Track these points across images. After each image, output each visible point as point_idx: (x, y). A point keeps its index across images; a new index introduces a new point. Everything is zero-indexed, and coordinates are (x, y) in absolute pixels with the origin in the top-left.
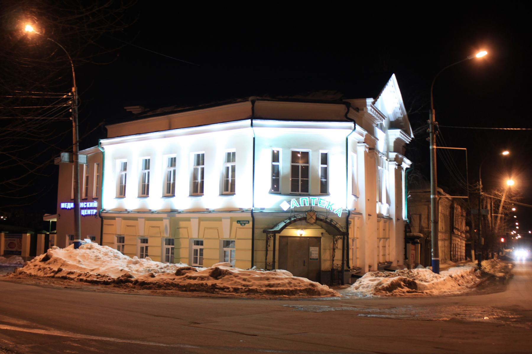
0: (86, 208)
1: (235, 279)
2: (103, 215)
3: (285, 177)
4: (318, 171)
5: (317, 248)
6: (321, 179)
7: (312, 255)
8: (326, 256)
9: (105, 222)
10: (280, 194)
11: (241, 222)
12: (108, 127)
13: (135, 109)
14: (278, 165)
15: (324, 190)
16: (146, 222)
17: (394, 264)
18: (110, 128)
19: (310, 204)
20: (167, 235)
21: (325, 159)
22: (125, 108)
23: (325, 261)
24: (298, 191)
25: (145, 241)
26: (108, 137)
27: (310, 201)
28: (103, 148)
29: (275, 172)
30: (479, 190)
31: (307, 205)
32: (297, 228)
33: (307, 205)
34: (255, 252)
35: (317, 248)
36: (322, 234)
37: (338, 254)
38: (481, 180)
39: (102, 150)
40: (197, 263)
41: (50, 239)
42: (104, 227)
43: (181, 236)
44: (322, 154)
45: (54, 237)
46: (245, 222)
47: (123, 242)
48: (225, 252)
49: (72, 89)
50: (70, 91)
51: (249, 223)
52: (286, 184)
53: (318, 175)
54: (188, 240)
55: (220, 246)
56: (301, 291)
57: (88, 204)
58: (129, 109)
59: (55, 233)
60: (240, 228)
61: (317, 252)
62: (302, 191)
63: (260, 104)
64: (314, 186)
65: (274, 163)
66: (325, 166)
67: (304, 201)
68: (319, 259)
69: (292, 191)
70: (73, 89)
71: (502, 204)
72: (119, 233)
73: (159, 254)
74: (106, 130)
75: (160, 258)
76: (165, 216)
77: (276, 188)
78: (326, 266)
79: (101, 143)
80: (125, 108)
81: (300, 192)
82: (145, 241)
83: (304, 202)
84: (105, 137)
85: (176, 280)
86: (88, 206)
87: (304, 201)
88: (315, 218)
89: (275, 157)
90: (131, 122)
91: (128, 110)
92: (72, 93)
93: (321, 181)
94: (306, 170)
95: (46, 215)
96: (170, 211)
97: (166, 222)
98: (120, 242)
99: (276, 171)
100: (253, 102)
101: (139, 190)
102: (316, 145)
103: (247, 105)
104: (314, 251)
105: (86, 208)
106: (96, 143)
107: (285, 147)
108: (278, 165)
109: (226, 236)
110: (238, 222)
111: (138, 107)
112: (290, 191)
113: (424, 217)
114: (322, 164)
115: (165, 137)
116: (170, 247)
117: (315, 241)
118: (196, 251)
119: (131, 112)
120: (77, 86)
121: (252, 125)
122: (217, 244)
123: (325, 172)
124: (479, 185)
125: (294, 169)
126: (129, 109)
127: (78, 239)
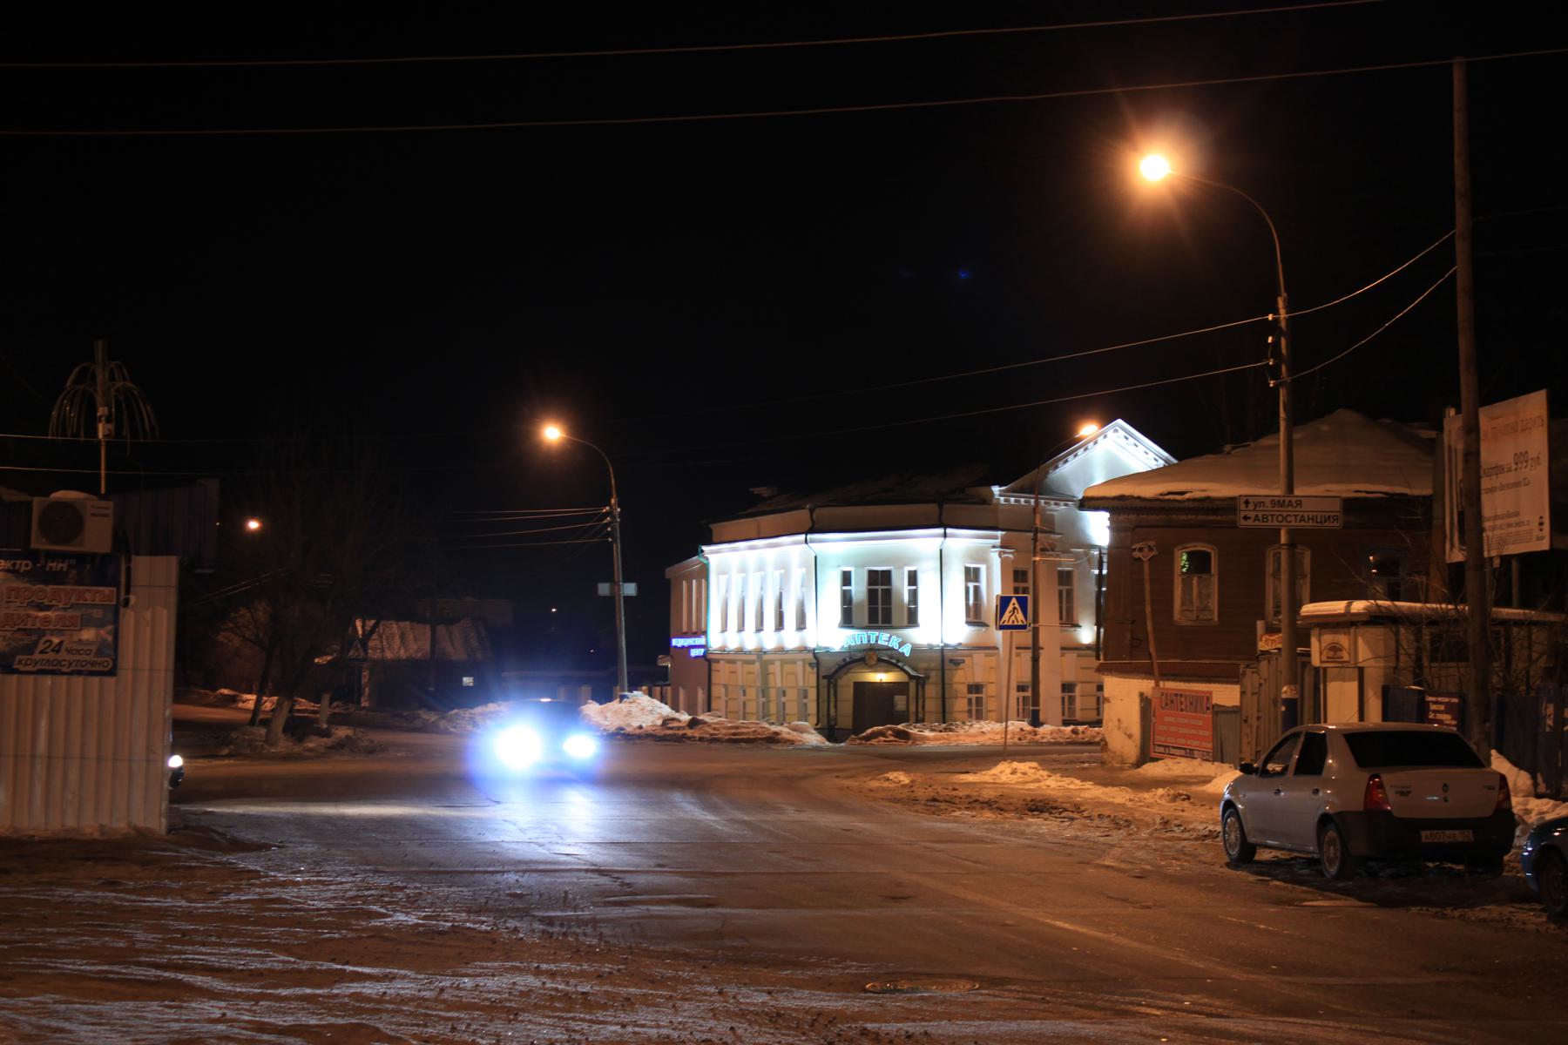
1: (707, 729)
2: (710, 657)
3: (860, 605)
4: (902, 594)
6: (909, 604)
7: (898, 707)
9: (714, 666)
10: (852, 627)
12: (712, 526)
13: (764, 491)
14: (850, 590)
15: (912, 619)
16: (745, 666)
18: (717, 528)
19: (869, 641)
21: (913, 578)
22: (751, 490)
24: (877, 623)
26: (715, 540)
27: (869, 637)
28: (707, 559)
29: (846, 598)
32: (876, 671)
33: (865, 642)
34: (940, 709)
35: (905, 697)
39: (705, 562)
44: (909, 572)
45: (666, 690)
48: (806, 704)
49: (610, 501)
50: (609, 504)
52: (862, 615)
53: (903, 600)
55: (799, 696)
56: (761, 739)
58: (757, 491)
59: (669, 685)
61: (905, 703)
62: (883, 623)
63: (824, 512)
64: (898, 615)
65: (845, 588)
66: (914, 588)
69: (870, 623)
70: (613, 501)
73: (755, 711)
74: (710, 531)
75: (755, 716)
77: (848, 620)
79: (702, 551)
80: (751, 490)
81: (880, 624)
83: (884, 638)
84: (710, 542)
85: (1009, 771)
87: (861, 638)
88: (875, 658)
89: (846, 578)
90: (747, 520)
91: (756, 493)
93: (909, 608)
94: (888, 594)
95: (660, 656)
97: (757, 667)
99: (848, 598)
100: (812, 511)
101: (776, 620)
102: (901, 560)
103: (802, 515)
106: (697, 552)
107: (859, 566)
108: (850, 590)
111: (765, 488)
112: (866, 623)
114: (910, 584)
115: (752, 548)
119: (759, 495)
120: (618, 496)
121: (806, 542)
123: (914, 596)
125: (872, 595)
126: (757, 491)
127: (624, 691)
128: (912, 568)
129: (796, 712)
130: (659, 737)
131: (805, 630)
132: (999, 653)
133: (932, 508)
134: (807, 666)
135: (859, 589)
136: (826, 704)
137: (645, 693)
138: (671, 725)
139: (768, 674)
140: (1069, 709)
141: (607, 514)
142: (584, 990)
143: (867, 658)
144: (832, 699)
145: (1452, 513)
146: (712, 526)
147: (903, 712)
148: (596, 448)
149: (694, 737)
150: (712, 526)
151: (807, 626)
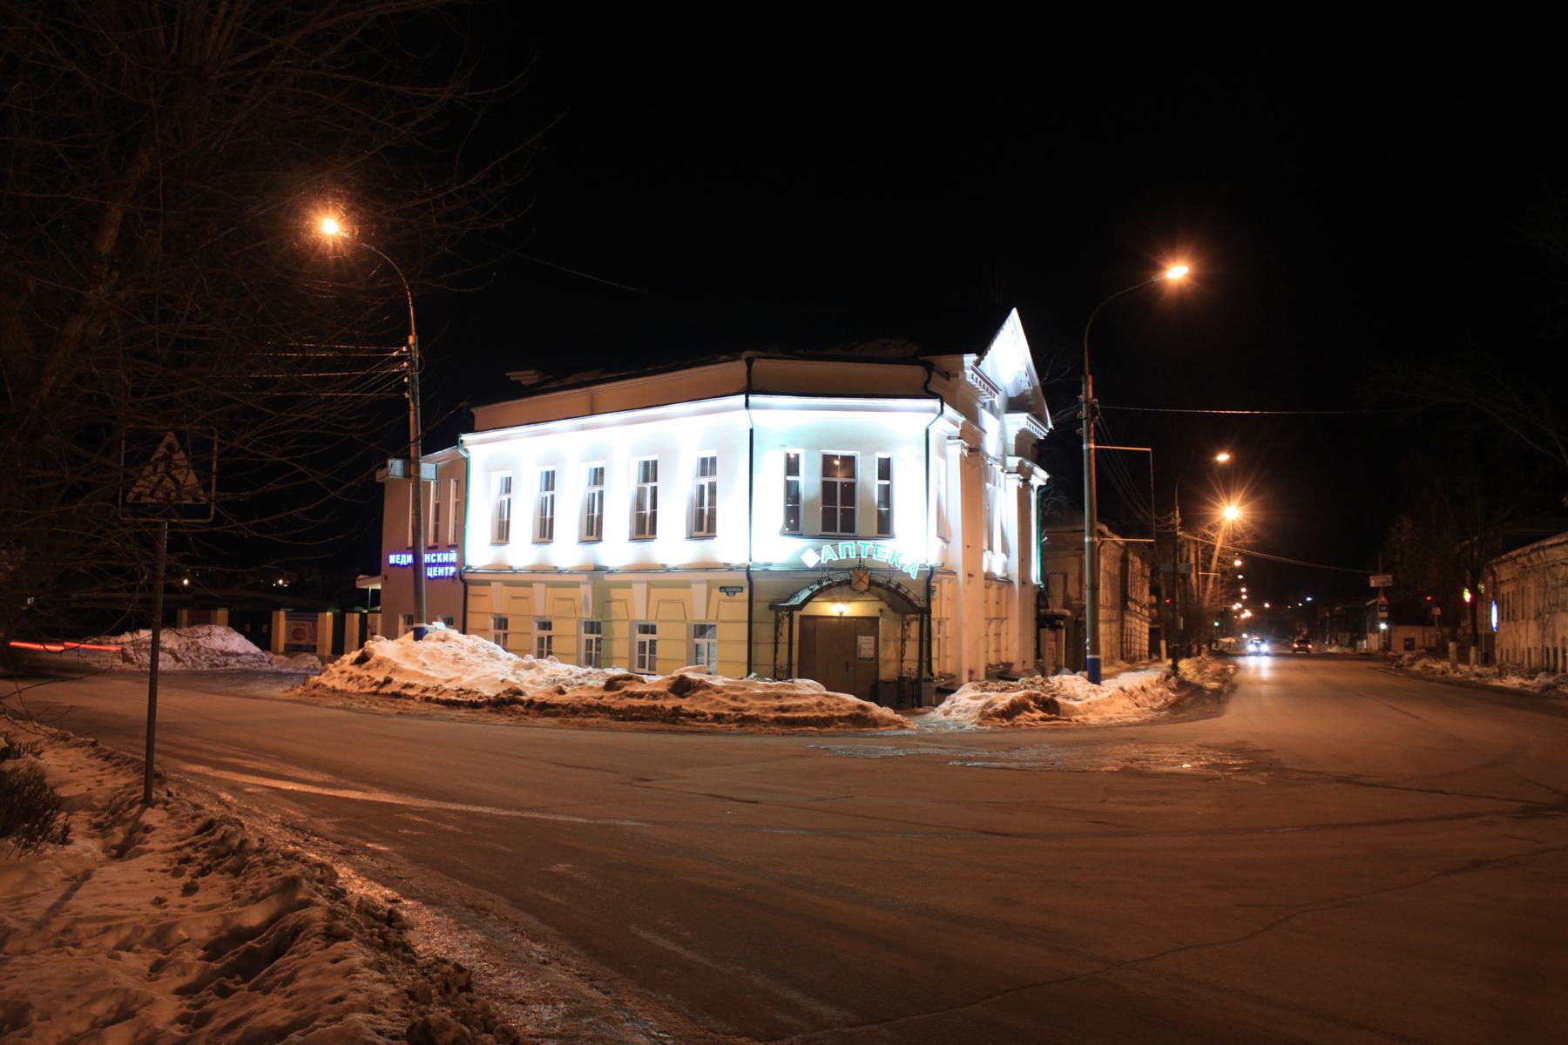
0: (434, 565)
2: (467, 577)
3: (810, 504)
4: (872, 492)
5: (872, 638)
6: (879, 507)
8: (889, 652)
9: (472, 589)
10: (801, 536)
11: (728, 590)
13: (527, 377)
14: (797, 482)
15: (884, 527)
16: (549, 589)
17: (1017, 668)
18: (480, 413)
20: (588, 615)
21: (885, 470)
23: (887, 661)
24: (836, 531)
25: (647, 629)
26: (476, 429)
27: (858, 549)
29: (792, 494)
30: (1174, 526)
31: (853, 556)
32: (835, 601)
33: (853, 556)
35: (872, 638)
36: (881, 611)
37: (912, 650)
38: (1178, 508)
40: (644, 667)
41: (369, 622)
42: (470, 599)
43: (614, 617)
46: (734, 590)
47: (506, 628)
49: (408, 340)
50: (406, 343)
51: (742, 591)
52: (812, 518)
54: (627, 625)
56: (841, 719)
57: (439, 556)
60: (725, 601)
61: (872, 646)
63: (764, 366)
64: (865, 519)
65: (790, 478)
66: (887, 482)
67: (847, 549)
68: (875, 660)
69: (824, 530)
70: (411, 340)
71: (1216, 553)
72: (497, 611)
74: (472, 417)
76: (584, 578)
77: (794, 522)
78: (888, 672)
79: (462, 441)
81: (839, 533)
82: (546, 626)
83: (846, 550)
84: (471, 429)
86: (439, 560)
87: (847, 549)
88: (866, 580)
89: (792, 466)
92: (409, 347)
94: (850, 491)
95: (361, 577)
96: (592, 569)
97: (586, 590)
98: (500, 628)
99: (793, 493)
100: (749, 362)
102: (870, 443)
104: (865, 644)
105: (434, 565)
109: (700, 616)
110: (722, 589)
112: (820, 531)
113: (1072, 578)
114: (880, 478)
115: (583, 428)
116: (593, 637)
117: (868, 625)
118: (642, 645)
120: (418, 333)
121: (747, 405)
122: (682, 632)
123: (886, 493)
124: (1175, 517)
125: (828, 489)
126: (514, 376)
128: (885, 455)
129: (685, 657)
130: (621, 711)
131: (715, 539)
132: (957, 579)
133: (917, 372)
134: (716, 592)
135: (810, 482)
136: (786, 646)
137: (1405, 644)
138: (630, 689)
139: (609, 602)
140: (543, 647)
141: (400, 359)
142: (205, 1029)
143: (855, 579)
144: (925, 638)
145: (1089, 471)
146: (474, 410)
147: (872, 659)
148: (390, 261)
149: (704, 714)
150: (474, 410)
151: (604, 537)
